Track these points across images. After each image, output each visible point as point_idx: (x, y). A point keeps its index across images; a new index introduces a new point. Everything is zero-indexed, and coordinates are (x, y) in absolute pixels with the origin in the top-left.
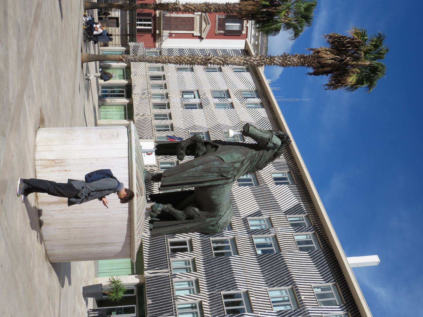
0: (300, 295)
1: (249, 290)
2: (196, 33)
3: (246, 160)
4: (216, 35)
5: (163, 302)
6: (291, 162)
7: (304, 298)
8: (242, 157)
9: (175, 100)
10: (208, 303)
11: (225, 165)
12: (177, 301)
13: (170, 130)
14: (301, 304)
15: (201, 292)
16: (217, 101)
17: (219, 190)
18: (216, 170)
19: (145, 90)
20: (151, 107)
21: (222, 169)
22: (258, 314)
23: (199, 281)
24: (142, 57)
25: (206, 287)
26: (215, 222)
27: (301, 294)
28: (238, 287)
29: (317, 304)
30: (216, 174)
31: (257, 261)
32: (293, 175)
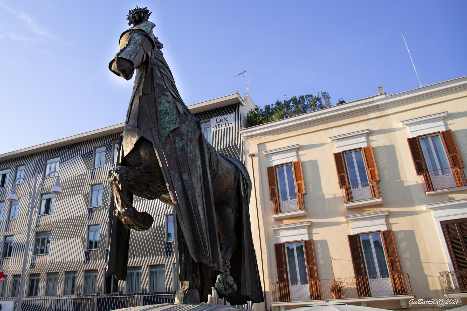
1: (166, 213)
6: (36, 157)
8: (167, 96)
12: (172, 290)
15: (164, 263)
23: (152, 264)
25: (156, 258)
28: (162, 224)
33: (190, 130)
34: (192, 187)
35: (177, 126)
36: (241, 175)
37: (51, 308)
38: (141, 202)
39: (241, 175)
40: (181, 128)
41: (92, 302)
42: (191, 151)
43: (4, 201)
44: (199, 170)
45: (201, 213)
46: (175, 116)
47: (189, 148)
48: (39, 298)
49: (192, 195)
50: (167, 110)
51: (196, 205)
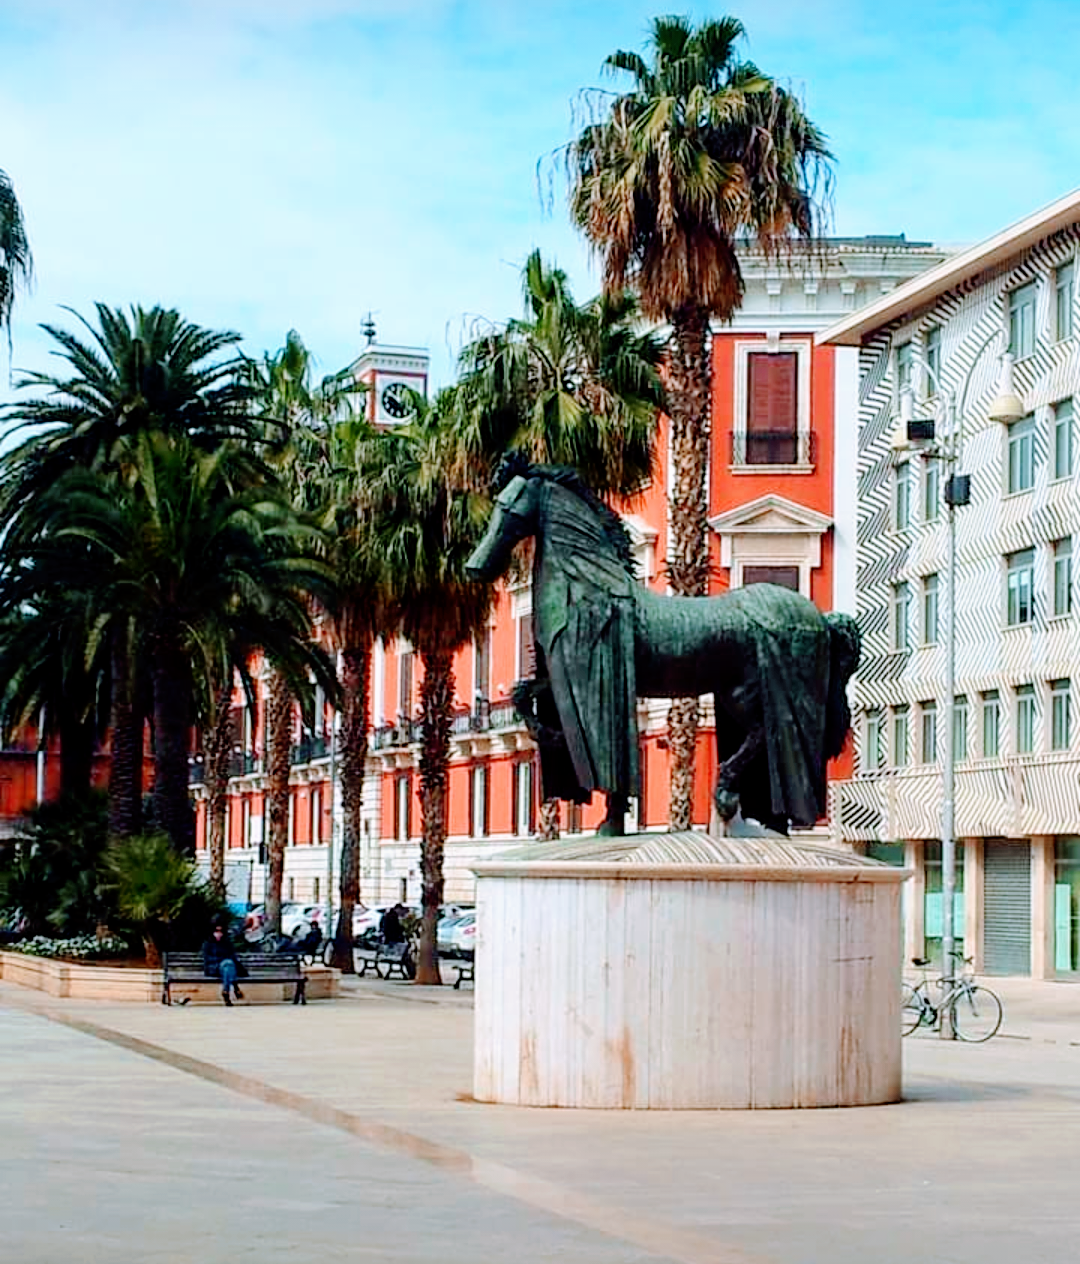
2: (808, 557)
4: (814, 470)
11: (572, 628)
16: (1043, 472)
17: (654, 636)
18: (585, 649)
20: (1062, 759)
21: (582, 633)
24: (675, 808)
26: (771, 639)
30: (598, 650)
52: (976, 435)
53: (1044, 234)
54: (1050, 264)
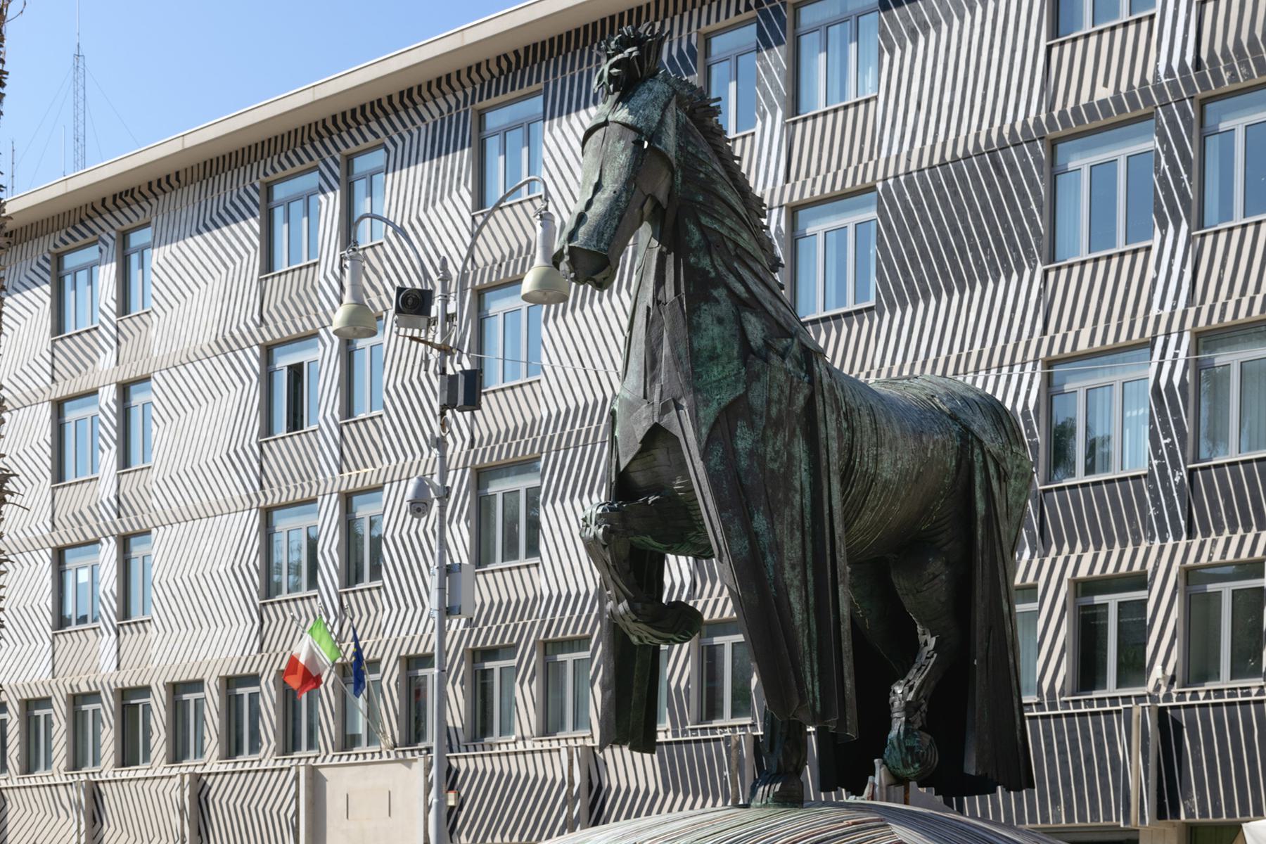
0: (1089, 107)
1: (1043, 354)
3: (732, 280)
5: (1062, 752)
6: (431, 105)
7: (1106, 84)
8: (717, 301)
9: (101, 661)
10: (1085, 550)
13: (255, 689)
14: (1134, 105)
15: (1030, 580)
19: (57, 800)
22: (1158, 318)
27: (1084, 99)
29: (1145, 25)
31: (910, 309)
32: (494, 100)
33: (775, 395)
34: (777, 548)
35: (740, 390)
36: (977, 451)
37: (572, 784)
38: (933, 302)
39: (977, 451)
40: (750, 395)
41: (734, 754)
42: (777, 453)
43: (316, 335)
44: (798, 497)
45: (797, 607)
46: (736, 362)
47: (769, 449)
48: (520, 747)
49: (774, 567)
50: (715, 348)
51: (783, 591)
52: (15, 412)
53: (108, 192)
54: (117, 226)
